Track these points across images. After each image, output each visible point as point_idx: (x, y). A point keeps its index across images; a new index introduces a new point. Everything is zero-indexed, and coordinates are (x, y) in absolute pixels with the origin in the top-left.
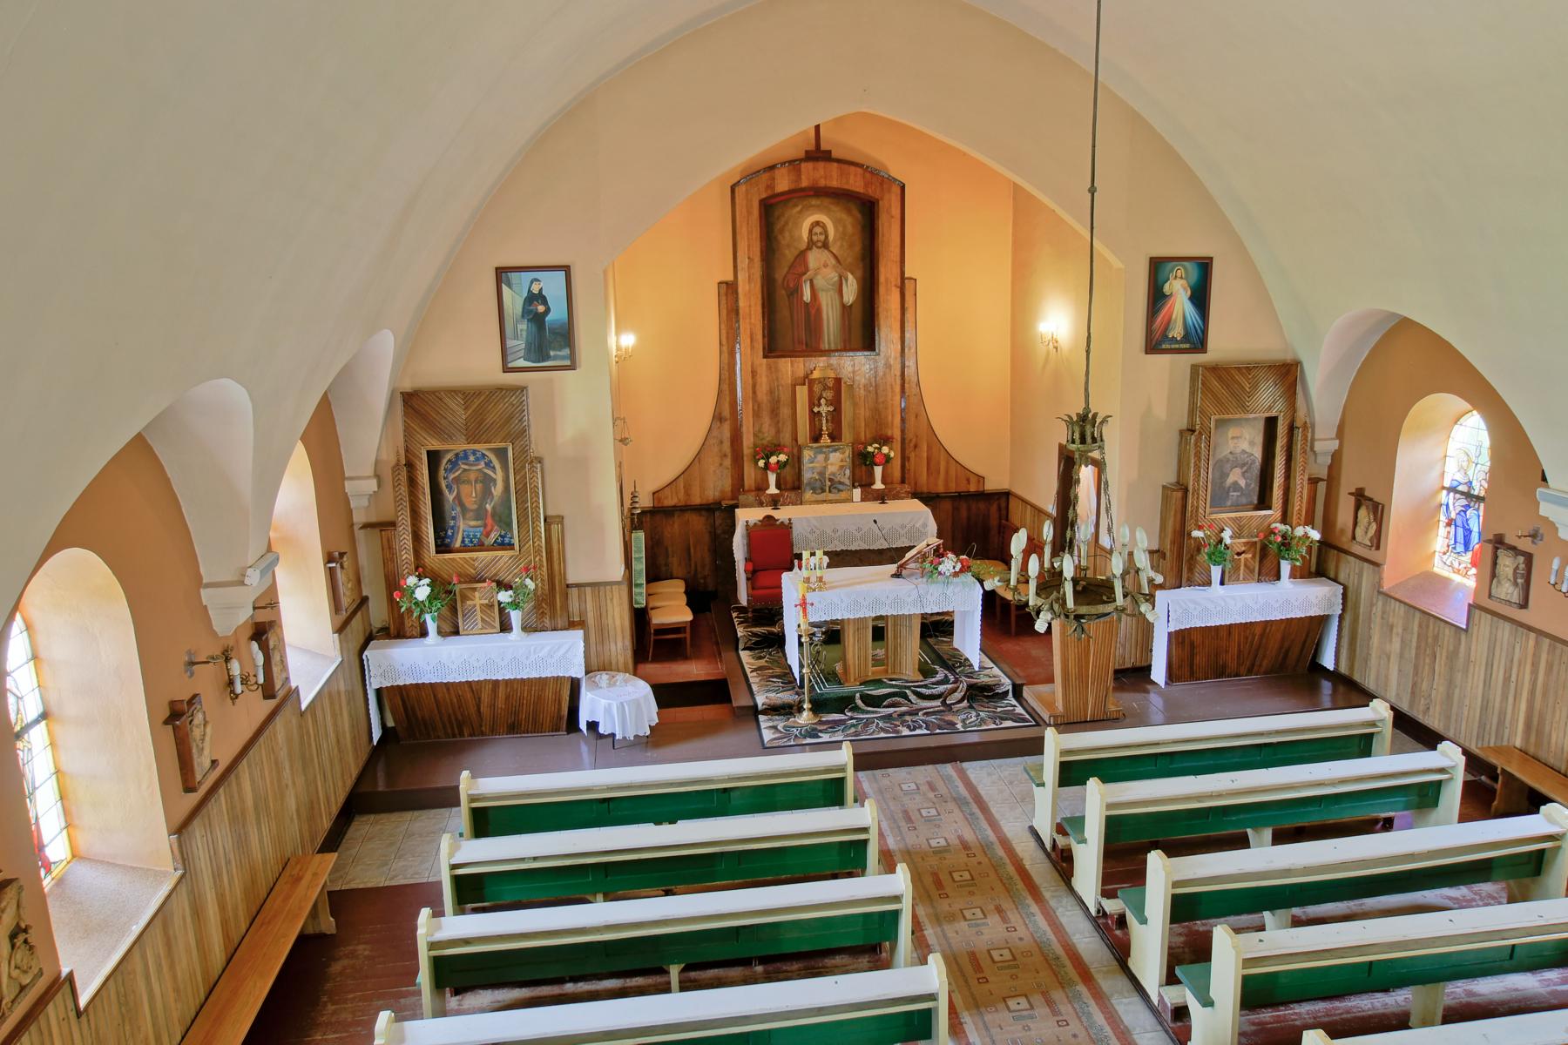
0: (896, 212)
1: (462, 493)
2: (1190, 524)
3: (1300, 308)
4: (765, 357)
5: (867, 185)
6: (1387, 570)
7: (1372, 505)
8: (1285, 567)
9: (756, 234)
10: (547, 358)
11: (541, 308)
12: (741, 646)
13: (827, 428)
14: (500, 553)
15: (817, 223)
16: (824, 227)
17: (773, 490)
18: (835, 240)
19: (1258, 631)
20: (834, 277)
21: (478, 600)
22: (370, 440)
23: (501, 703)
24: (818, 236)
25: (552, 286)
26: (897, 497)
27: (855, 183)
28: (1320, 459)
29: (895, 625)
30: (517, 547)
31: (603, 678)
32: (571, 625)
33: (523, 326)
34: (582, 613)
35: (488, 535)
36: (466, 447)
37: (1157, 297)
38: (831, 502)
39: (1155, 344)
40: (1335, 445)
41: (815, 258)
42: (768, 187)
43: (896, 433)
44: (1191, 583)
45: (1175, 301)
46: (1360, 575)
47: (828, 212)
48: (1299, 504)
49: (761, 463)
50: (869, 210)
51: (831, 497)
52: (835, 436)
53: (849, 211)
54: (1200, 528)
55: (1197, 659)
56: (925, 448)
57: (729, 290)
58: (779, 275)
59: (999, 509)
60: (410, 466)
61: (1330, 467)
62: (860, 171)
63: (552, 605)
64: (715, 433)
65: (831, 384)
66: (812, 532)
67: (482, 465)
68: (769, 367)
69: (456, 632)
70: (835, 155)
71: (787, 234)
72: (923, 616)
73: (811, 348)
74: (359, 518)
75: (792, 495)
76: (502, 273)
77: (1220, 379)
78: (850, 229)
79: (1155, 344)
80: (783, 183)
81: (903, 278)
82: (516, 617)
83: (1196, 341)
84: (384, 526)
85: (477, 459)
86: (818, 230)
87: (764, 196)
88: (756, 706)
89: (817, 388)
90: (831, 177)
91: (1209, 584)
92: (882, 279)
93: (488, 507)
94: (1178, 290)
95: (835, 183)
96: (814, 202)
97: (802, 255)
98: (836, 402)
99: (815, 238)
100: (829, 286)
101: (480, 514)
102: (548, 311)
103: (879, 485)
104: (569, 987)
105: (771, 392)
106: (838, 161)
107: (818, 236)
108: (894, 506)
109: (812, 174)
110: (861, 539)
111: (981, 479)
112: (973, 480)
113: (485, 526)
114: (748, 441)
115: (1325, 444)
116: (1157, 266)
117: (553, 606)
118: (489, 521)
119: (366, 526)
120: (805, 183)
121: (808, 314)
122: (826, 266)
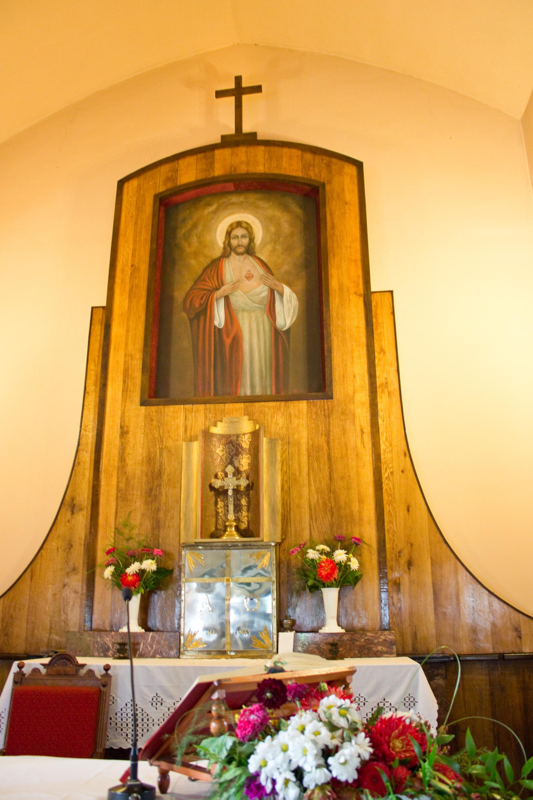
0: (352, 197)
4: (143, 403)
9: (146, 236)
13: (233, 510)
15: (239, 224)
16: (248, 228)
18: (264, 244)
20: (263, 291)
27: (291, 166)
41: (233, 268)
42: (168, 179)
47: (254, 209)
50: (311, 196)
53: (286, 208)
57: (103, 319)
62: (295, 152)
64: (61, 529)
68: (149, 419)
71: (194, 240)
73: (220, 382)
78: (286, 228)
81: (367, 296)
86: (239, 232)
90: (259, 163)
92: (334, 284)
96: (234, 199)
97: (216, 264)
99: (234, 242)
100: (254, 303)
104: (474, 658)
105: (150, 459)
114: (105, 541)
120: (218, 171)
122: (249, 277)
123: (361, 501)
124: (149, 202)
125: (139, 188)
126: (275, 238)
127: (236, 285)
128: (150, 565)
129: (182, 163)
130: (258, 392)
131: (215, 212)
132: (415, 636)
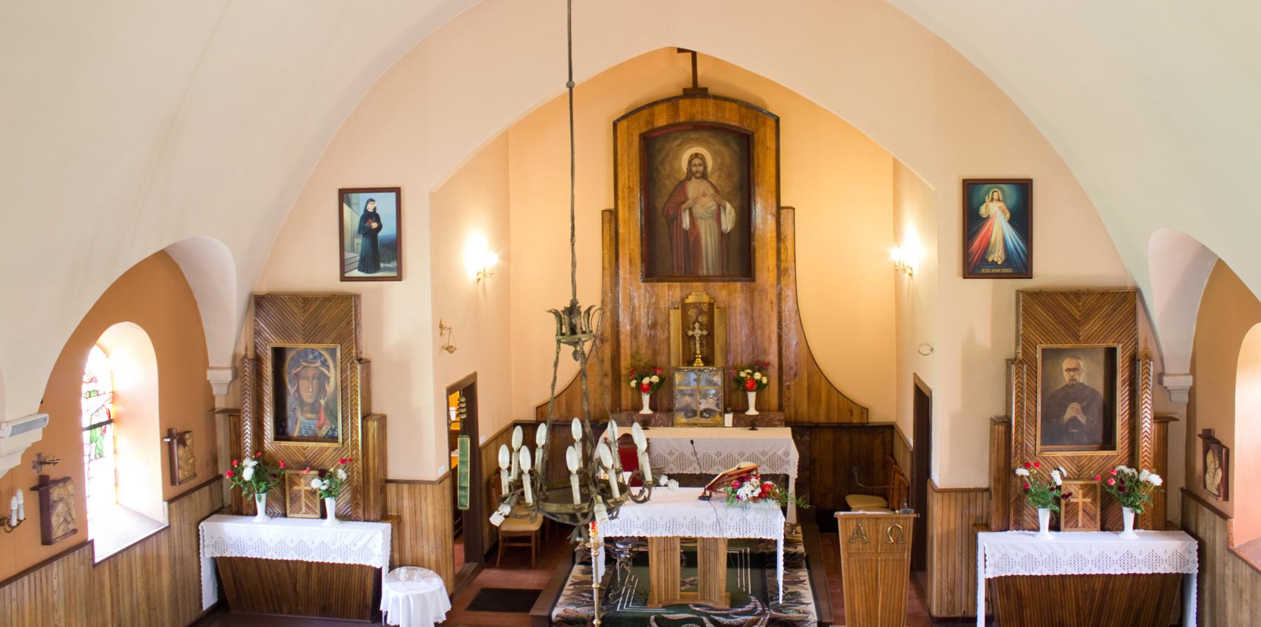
1: (301, 390)
2: (1015, 460)
3: (1119, 227)
5: (742, 118)
6: (1236, 524)
7: (1218, 447)
8: (1129, 516)
9: (636, 166)
10: (377, 269)
11: (374, 225)
12: (578, 560)
14: (326, 445)
15: (696, 155)
16: (703, 159)
17: (646, 410)
19: (1098, 585)
20: (712, 205)
21: (302, 487)
22: (227, 335)
23: (313, 585)
24: (696, 170)
25: (384, 205)
26: (770, 424)
27: (731, 118)
28: (1175, 397)
29: (704, 549)
30: (340, 440)
31: (402, 571)
32: (384, 517)
33: (359, 241)
34: (400, 509)
35: (320, 428)
36: (303, 346)
37: (972, 221)
38: (702, 425)
39: (975, 265)
40: (1187, 381)
41: (694, 188)
43: (773, 358)
44: (1019, 526)
45: (995, 222)
46: (1214, 528)
47: (706, 144)
48: (1146, 445)
49: (633, 383)
51: (703, 421)
52: (708, 361)
53: (727, 144)
54: (1027, 466)
55: (1027, 613)
56: (805, 376)
57: (611, 217)
58: (660, 204)
59: (884, 443)
60: (258, 360)
61: (1189, 405)
62: (735, 106)
63: (366, 497)
65: (705, 309)
66: (671, 453)
67: (318, 364)
69: (285, 515)
70: (712, 91)
71: (667, 165)
72: (732, 542)
73: (689, 274)
74: (220, 404)
75: (664, 416)
76: (344, 195)
77: (1044, 305)
78: (728, 160)
79: (975, 265)
80: (662, 120)
82: (330, 503)
83: (1019, 265)
84: (234, 414)
85: (315, 358)
86: (697, 161)
87: (644, 130)
88: (550, 617)
89: (692, 313)
90: (706, 112)
91: (1038, 529)
93: (322, 402)
94: (996, 212)
95: (711, 118)
96: (693, 135)
97: (682, 185)
98: (710, 327)
99: (694, 169)
100: (706, 214)
101: (314, 408)
102: (380, 227)
103: (752, 411)
106: (715, 97)
107: (696, 170)
108: (763, 433)
109: (688, 110)
110: (721, 463)
111: (865, 411)
112: (856, 411)
113: (319, 419)
114: (625, 362)
115: (1178, 380)
116: (972, 191)
117: (370, 496)
118: (323, 414)
119: (223, 411)
120: (682, 118)
121: (687, 240)
122: (704, 195)
123: (770, 341)
124: (636, 139)
125: (628, 127)
126: (720, 167)
127: (696, 200)
128: (655, 379)
129: (657, 109)
130: (711, 273)
131: (680, 145)
132: (796, 412)
